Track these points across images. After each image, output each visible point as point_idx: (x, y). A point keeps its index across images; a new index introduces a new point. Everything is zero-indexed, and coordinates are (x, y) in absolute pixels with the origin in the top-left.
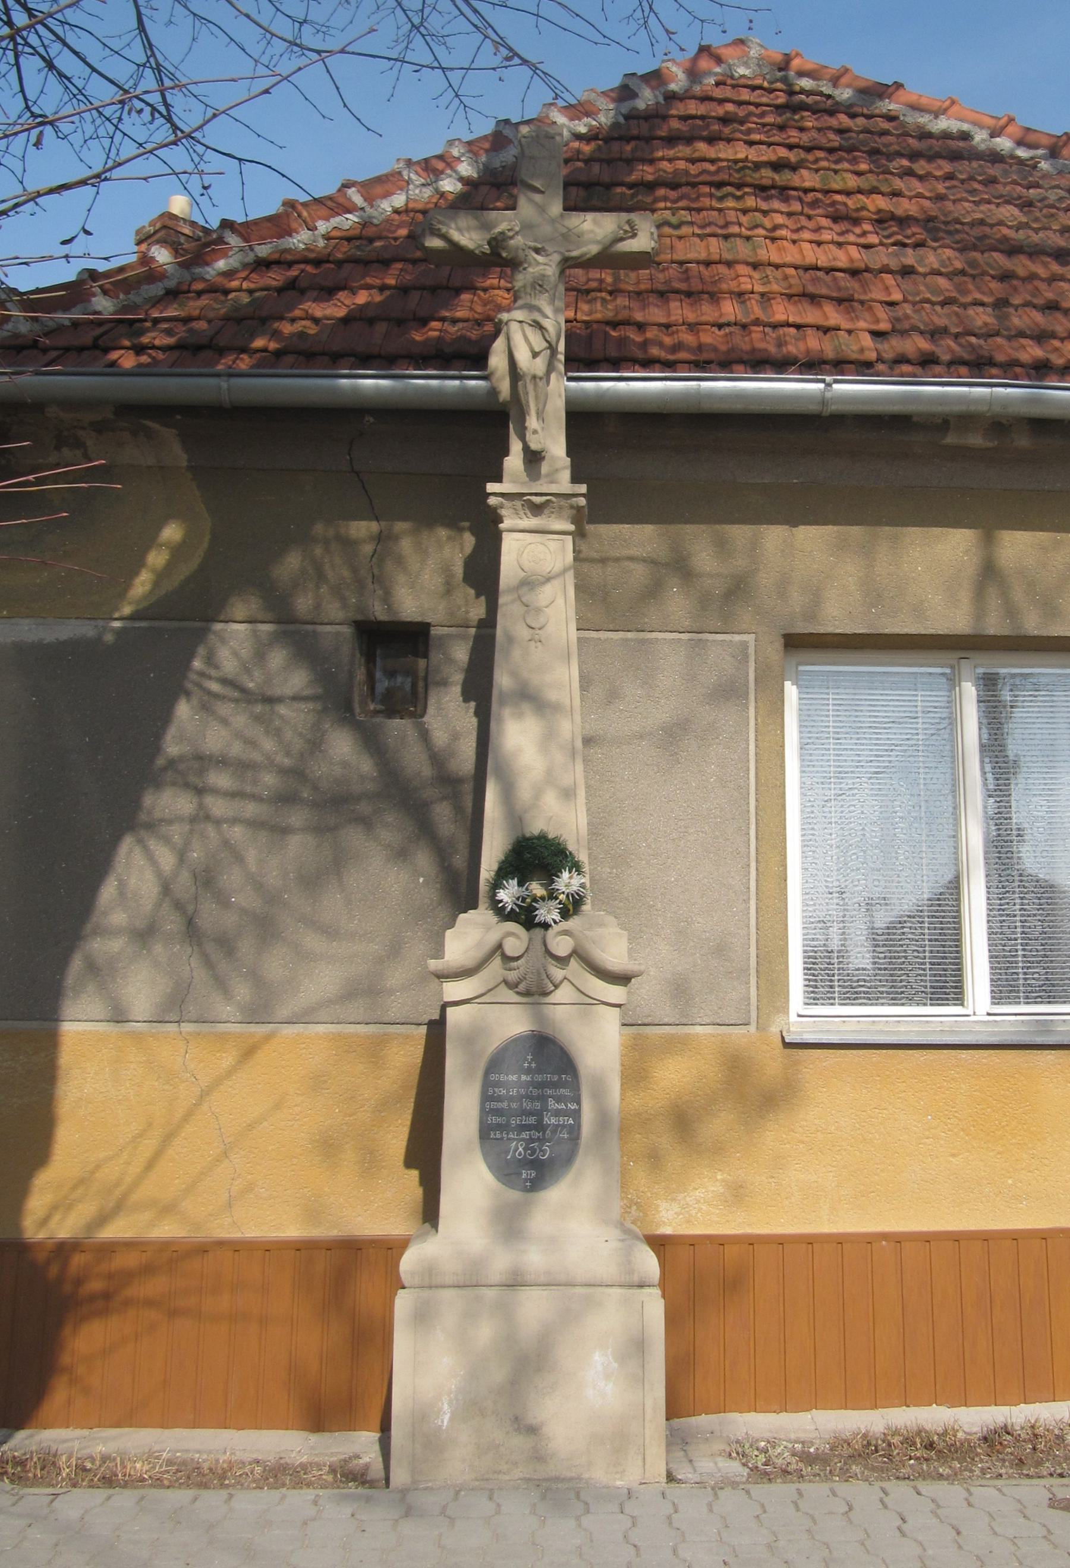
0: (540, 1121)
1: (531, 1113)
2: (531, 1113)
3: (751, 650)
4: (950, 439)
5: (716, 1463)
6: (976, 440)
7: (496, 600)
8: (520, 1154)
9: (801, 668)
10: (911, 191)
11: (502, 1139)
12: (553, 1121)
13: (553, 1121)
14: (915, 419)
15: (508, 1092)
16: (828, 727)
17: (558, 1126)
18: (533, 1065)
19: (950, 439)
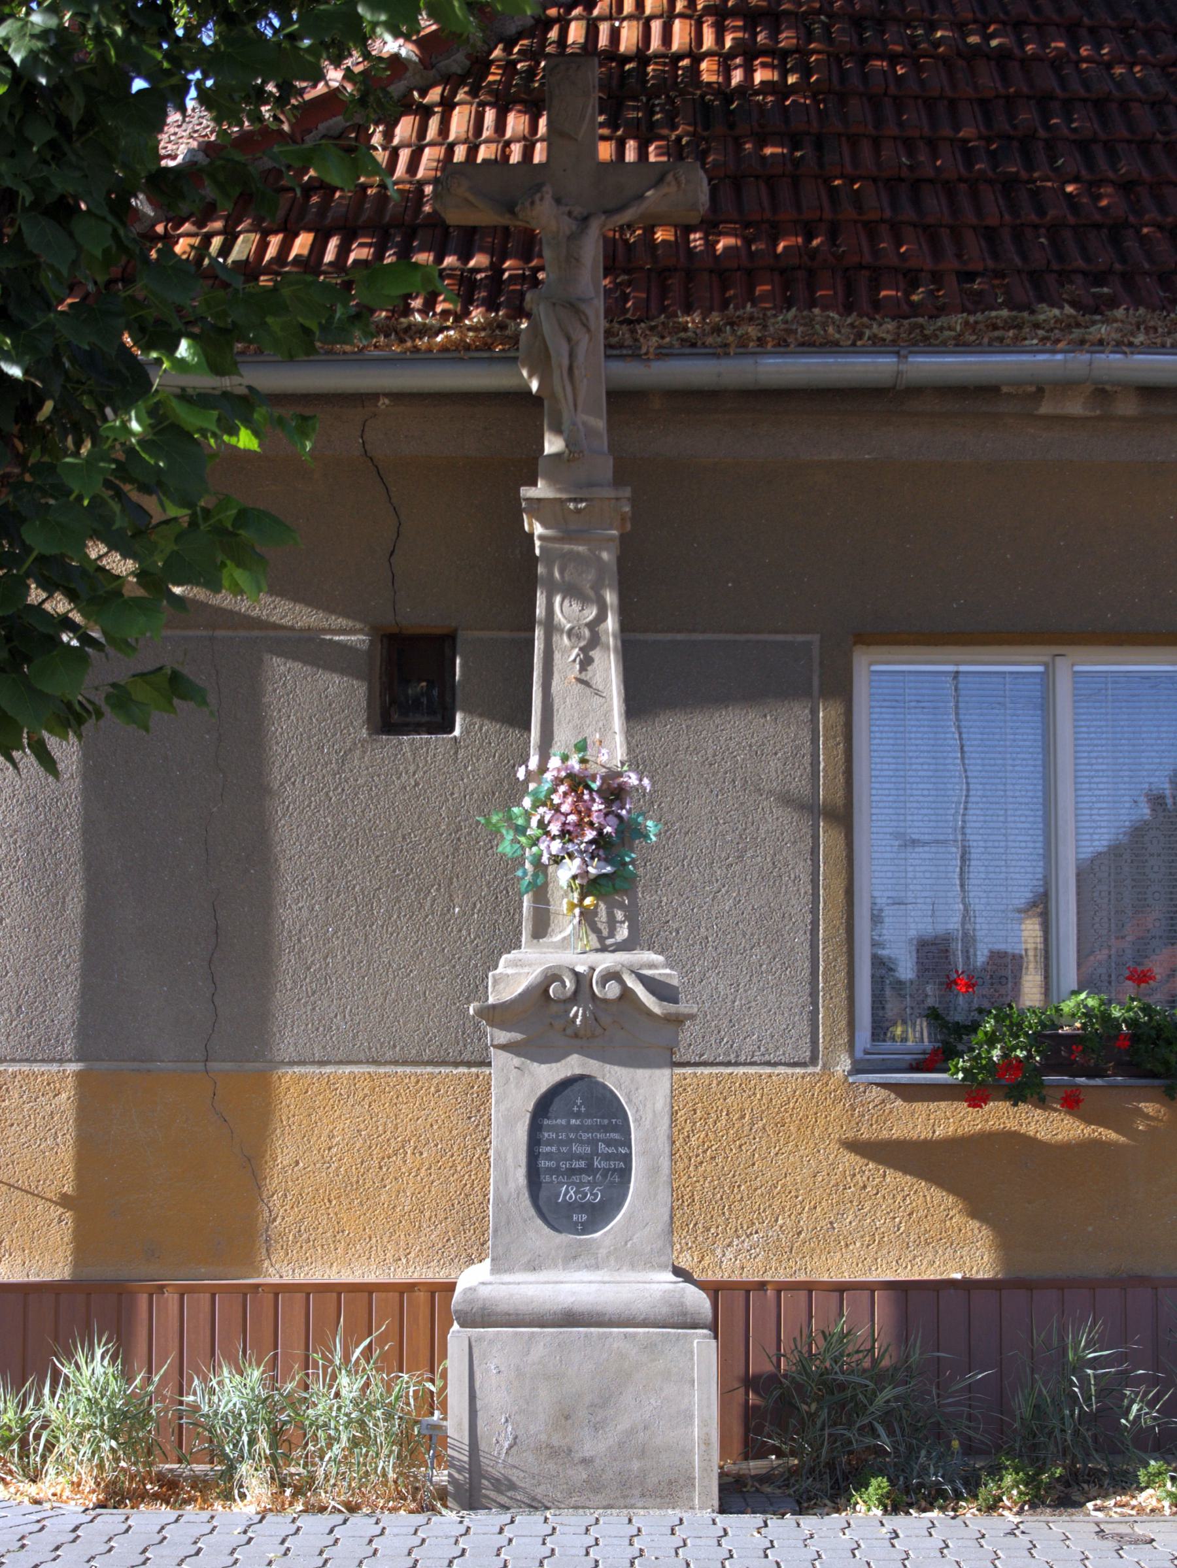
0: (590, 1164)
1: (580, 1157)
2: (580, 1157)
3: (816, 652)
4: (1045, 409)
5: (641, 780)
6: (1075, 407)
7: (879, 1161)
8: (571, 1198)
9: (874, 668)
10: (495, 982)
11: (552, 1182)
12: (604, 1164)
13: (604, 1164)
14: (1005, 389)
15: (557, 1136)
16: (1107, 714)
17: (609, 1169)
18: (583, 1109)
19: (1045, 409)
